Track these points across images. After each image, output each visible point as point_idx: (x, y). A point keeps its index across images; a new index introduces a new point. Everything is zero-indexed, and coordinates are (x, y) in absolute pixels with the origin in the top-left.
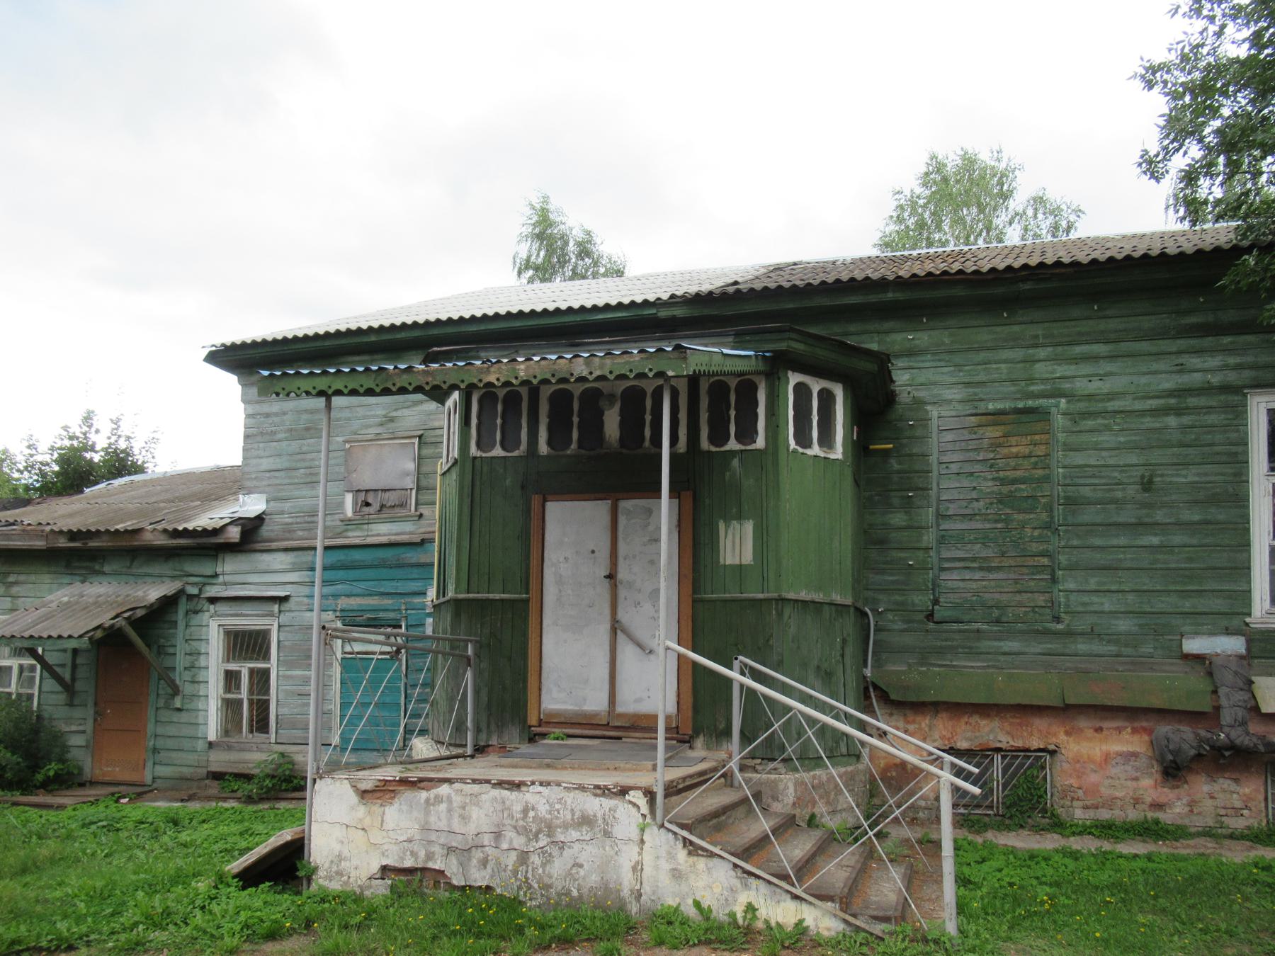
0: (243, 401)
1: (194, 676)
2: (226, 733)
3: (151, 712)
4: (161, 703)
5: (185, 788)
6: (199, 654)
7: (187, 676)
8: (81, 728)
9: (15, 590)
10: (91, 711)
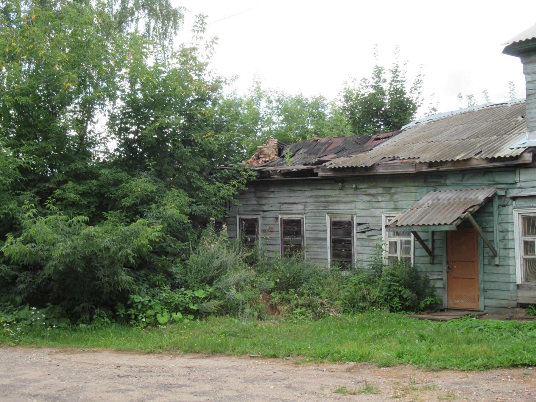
0: (525, 73)
1: (505, 245)
2: (527, 279)
3: (480, 268)
4: (486, 262)
5: (501, 311)
6: (508, 231)
7: (501, 245)
8: (440, 277)
9: (396, 197)
10: (445, 267)
